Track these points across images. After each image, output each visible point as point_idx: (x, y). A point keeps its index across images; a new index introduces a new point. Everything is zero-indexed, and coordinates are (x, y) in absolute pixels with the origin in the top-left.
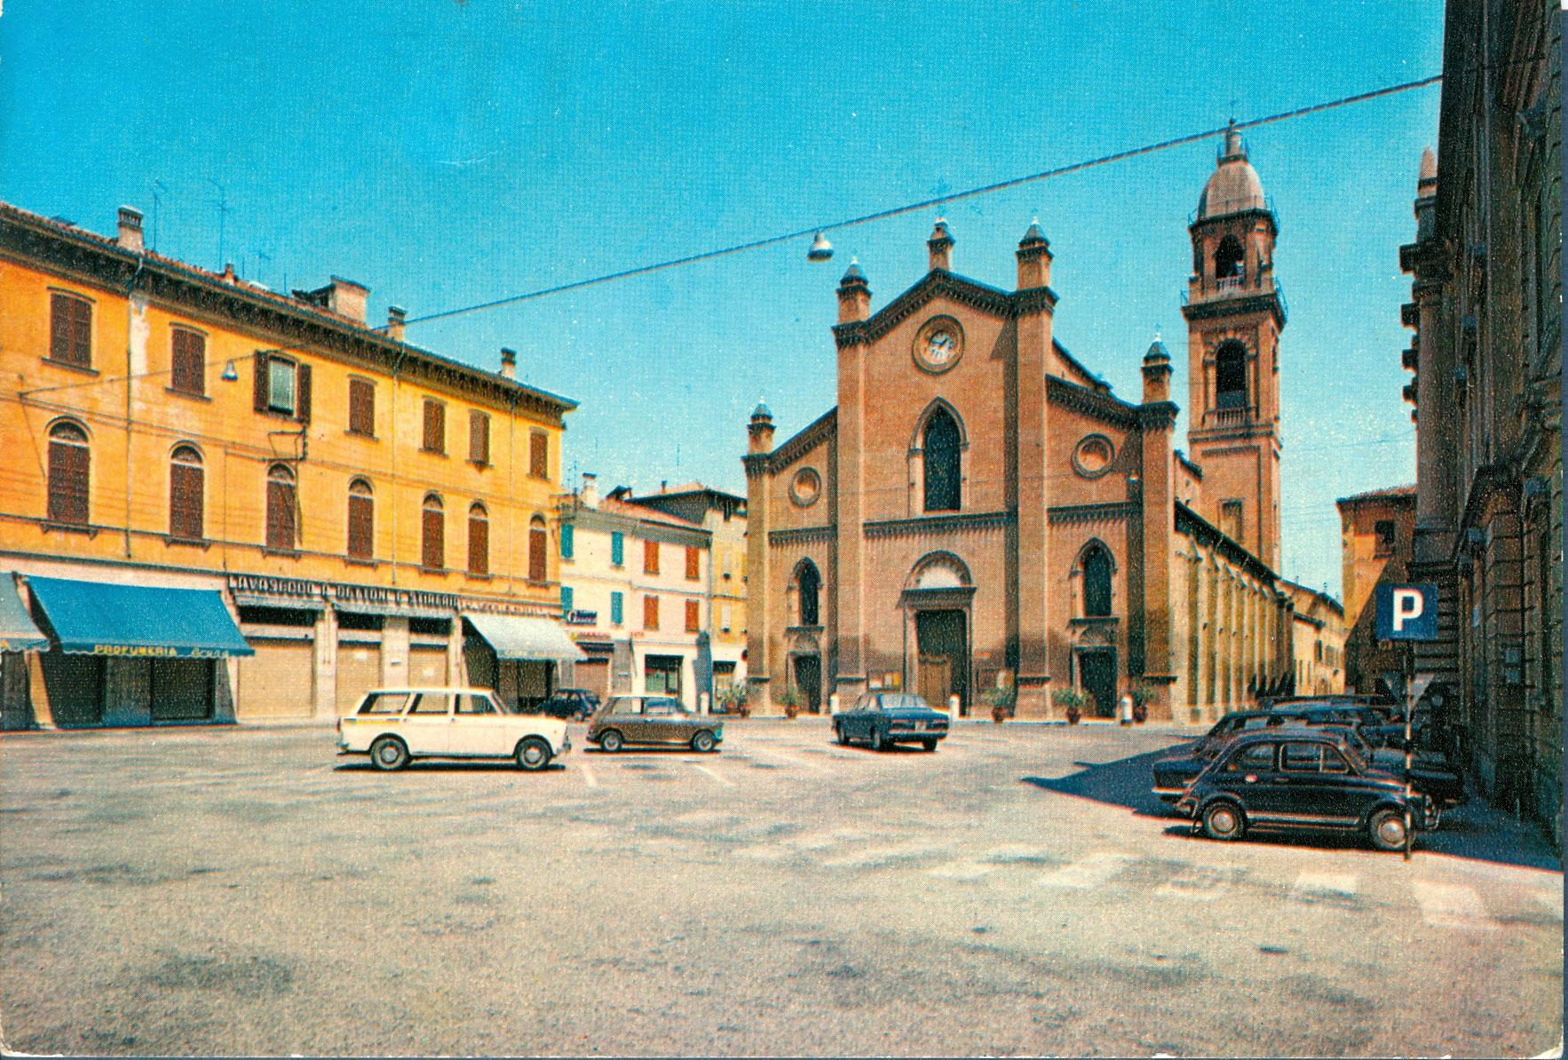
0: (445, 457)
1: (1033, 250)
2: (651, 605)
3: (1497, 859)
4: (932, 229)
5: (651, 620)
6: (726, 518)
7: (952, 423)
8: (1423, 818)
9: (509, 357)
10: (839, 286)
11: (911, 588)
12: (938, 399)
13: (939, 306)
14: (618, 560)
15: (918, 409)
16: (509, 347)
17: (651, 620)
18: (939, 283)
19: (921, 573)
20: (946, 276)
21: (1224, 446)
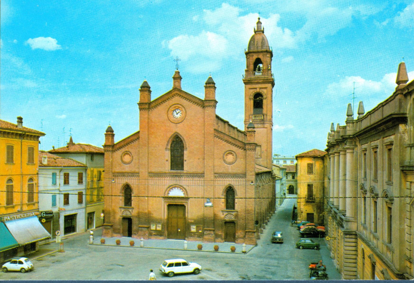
0: (77, 214)
1: (210, 84)
2: (67, 197)
3: (177, 239)
4: (174, 73)
5: (66, 202)
6: (171, 50)
7: (181, 141)
8: (156, 231)
9: (20, 120)
10: (140, 89)
11: (166, 196)
12: (176, 132)
13: (176, 99)
14: (54, 183)
15: (170, 135)
16: (19, 116)
17: (66, 202)
18: (177, 91)
19: (170, 191)
20: (180, 90)
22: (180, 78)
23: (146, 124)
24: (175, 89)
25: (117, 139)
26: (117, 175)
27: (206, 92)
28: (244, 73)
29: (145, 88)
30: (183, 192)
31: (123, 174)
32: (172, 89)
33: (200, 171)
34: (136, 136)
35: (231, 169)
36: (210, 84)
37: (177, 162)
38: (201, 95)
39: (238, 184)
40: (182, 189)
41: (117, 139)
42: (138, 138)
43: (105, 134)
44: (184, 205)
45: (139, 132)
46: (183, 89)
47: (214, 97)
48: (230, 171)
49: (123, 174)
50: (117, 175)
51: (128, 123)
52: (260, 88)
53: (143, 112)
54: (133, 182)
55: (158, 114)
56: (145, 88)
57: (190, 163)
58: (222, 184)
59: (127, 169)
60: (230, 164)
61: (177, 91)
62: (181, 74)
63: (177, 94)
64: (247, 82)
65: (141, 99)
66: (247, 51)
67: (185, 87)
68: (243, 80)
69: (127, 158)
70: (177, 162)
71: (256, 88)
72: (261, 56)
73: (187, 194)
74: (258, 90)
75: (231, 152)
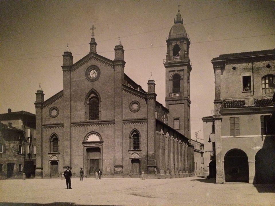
1: (119, 49)
13: (93, 62)
18: (93, 55)
21: (174, 102)
22: (96, 44)
23: (68, 83)
24: (91, 53)
25: (46, 98)
26: (46, 126)
27: (115, 54)
28: (165, 58)
29: (68, 55)
30: (99, 138)
31: (52, 126)
32: (89, 53)
33: (111, 119)
34: (60, 95)
35: (135, 116)
36: (119, 49)
37: (94, 113)
38: (111, 56)
39: (142, 128)
40: (98, 135)
41: (46, 98)
42: (63, 95)
43: (36, 94)
44: (99, 148)
45: (63, 91)
46: (98, 54)
47: (154, 91)
48: (135, 118)
49: (52, 126)
50: (46, 126)
51: (54, 85)
52: (178, 71)
53: (66, 73)
54: (57, 131)
55: (79, 75)
56: (68, 55)
57: (104, 114)
58: (129, 128)
59: (53, 121)
60: (99, 74)
61: (93, 55)
62: (96, 41)
63: (92, 57)
64: (167, 65)
65: (64, 63)
66: (168, 38)
67: (100, 51)
68: (164, 64)
69: (54, 113)
70: (94, 113)
71: (174, 71)
72: (178, 43)
73: (102, 139)
74: (176, 72)
75: (136, 103)
